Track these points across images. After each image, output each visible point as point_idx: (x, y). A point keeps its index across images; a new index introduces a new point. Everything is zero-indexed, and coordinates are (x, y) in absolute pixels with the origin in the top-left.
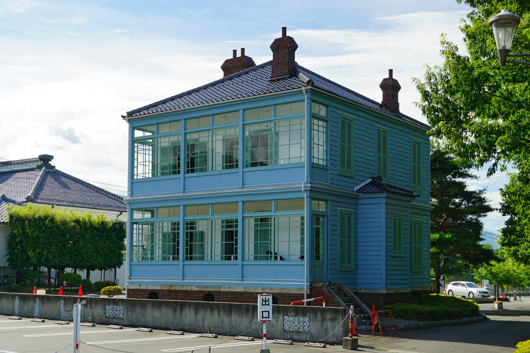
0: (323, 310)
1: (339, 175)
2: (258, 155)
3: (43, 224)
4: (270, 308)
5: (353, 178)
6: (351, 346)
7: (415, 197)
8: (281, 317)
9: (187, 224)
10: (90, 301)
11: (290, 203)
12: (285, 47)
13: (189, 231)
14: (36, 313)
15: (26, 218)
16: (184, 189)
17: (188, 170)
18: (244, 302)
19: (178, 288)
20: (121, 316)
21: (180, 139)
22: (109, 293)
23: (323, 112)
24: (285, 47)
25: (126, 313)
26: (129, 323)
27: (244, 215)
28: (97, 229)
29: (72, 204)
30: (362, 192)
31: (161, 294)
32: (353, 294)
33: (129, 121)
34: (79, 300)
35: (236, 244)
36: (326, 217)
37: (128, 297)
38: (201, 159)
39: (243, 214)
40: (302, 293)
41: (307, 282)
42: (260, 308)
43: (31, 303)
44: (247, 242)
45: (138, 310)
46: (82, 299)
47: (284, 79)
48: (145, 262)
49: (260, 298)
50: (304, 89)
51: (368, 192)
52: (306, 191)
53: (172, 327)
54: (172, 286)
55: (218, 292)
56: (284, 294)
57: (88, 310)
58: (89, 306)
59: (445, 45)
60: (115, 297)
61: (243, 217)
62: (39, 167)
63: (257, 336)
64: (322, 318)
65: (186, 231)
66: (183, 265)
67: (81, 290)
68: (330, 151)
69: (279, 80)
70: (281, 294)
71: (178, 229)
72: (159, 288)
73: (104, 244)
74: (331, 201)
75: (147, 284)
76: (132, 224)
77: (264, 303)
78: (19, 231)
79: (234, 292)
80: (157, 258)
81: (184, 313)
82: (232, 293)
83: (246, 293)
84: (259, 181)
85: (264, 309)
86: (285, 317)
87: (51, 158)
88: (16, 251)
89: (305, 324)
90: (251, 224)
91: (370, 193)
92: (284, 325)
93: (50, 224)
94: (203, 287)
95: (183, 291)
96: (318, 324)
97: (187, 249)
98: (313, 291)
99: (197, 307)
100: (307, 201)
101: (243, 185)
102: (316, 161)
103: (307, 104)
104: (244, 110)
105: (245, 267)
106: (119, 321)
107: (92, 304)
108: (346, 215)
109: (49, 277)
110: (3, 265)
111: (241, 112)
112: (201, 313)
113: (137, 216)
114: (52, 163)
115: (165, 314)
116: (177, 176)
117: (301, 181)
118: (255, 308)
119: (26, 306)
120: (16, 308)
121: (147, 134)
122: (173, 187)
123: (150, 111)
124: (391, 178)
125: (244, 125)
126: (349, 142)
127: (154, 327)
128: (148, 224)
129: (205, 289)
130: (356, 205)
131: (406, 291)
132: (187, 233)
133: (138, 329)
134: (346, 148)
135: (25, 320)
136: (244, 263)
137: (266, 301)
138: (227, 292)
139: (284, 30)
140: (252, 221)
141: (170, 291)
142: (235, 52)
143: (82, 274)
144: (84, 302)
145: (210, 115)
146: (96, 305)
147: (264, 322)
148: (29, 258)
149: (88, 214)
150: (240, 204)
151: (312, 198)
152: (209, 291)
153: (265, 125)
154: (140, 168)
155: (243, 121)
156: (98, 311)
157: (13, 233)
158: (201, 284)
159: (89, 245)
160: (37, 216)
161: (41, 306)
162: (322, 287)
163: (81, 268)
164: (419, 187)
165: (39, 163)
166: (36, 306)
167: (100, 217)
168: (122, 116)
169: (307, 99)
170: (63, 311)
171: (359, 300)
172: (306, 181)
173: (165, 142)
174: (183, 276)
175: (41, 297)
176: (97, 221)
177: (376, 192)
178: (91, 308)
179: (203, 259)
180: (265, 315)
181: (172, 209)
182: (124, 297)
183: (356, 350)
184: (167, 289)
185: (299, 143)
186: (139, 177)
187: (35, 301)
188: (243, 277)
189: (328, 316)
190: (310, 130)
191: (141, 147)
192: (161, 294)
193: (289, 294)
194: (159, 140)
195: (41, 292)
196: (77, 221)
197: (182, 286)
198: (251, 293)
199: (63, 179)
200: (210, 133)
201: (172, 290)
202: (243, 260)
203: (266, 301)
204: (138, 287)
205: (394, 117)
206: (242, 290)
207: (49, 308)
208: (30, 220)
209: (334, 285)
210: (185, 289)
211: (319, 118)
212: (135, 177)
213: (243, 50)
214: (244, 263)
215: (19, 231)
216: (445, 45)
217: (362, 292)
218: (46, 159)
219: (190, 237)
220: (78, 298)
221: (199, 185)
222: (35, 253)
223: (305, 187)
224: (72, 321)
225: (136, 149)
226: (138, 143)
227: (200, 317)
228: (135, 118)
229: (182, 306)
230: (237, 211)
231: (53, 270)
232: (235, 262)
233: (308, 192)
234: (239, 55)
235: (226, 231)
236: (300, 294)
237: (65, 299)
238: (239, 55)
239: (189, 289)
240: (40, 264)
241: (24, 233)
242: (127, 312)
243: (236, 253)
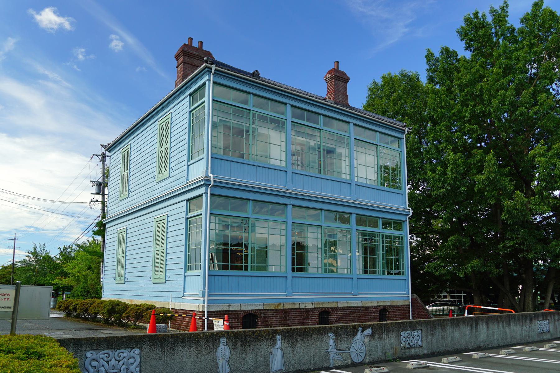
20: (420, 343)
25: (424, 338)
31: (262, 315)
34: (360, 329)
40: (407, 304)
46: (364, 328)
54: (280, 304)
55: (334, 308)
58: (377, 336)
60: (497, 309)
89: (132, 360)
95: (294, 309)
107: (382, 332)
129: (321, 306)
138: (345, 307)
144: (369, 331)
152: (384, 306)
161: (289, 350)
166: (275, 351)
170: (332, 349)
178: (380, 339)
179: (293, 270)
184: (273, 308)
187: (274, 342)
192: (262, 315)
198: (367, 307)
201: (279, 310)
210: (297, 307)
220: (359, 326)
236: (406, 305)
237: (284, 334)
239: (302, 306)
242: (427, 336)
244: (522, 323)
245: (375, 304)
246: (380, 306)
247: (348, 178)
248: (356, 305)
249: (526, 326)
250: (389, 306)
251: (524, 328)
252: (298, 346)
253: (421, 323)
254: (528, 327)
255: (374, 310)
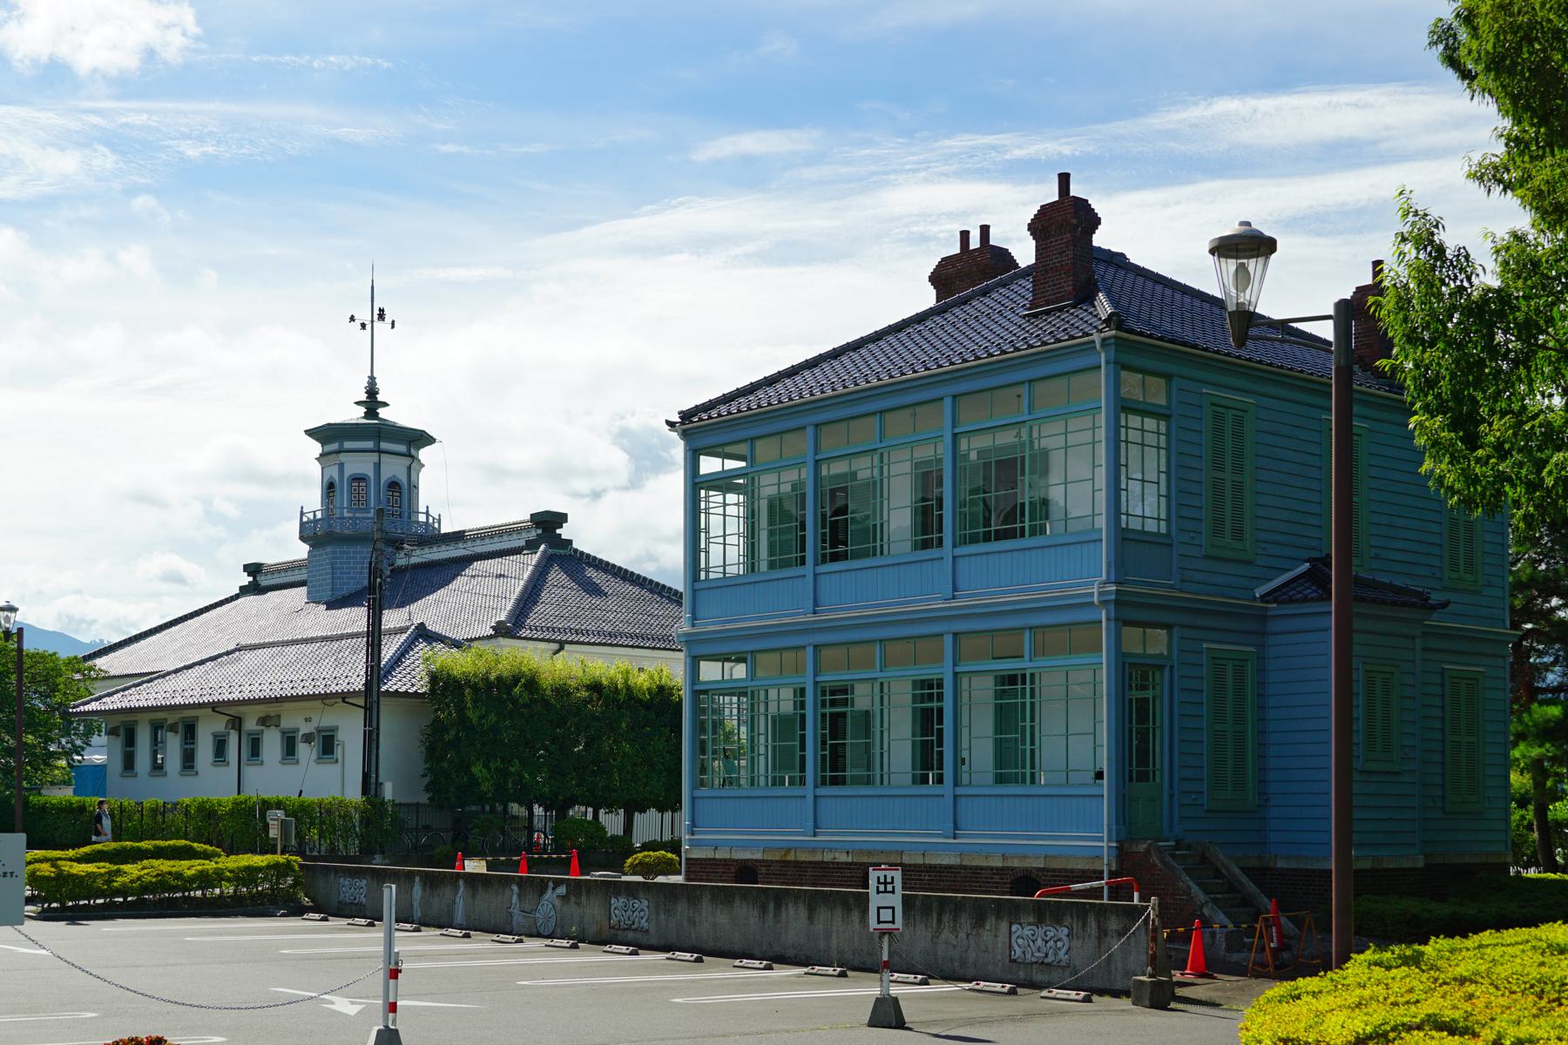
0: (1102, 911)
1: (1207, 557)
2: (1001, 509)
3: (511, 697)
4: (896, 900)
5: (1250, 563)
6: (1151, 1000)
7: (1433, 608)
8: (1004, 925)
9: (824, 693)
10: (576, 888)
11: (1060, 631)
12: (1065, 222)
13: (828, 710)
14: (459, 917)
15: (468, 682)
16: (816, 604)
17: (824, 556)
18: (840, 883)
19: (803, 857)
21: (803, 476)
22: (645, 869)
23: (1157, 394)
24: (1065, 222)
26: (662, 942)
27: (958, 669)
28: (647, 706)
29: (611, 640)
30: (1275, 601)
32: (1237, 871)
33: (685, 435)
34: (551, 885)
35: (940, 744)
36: (1167, 670)
37: (687, 879)
38: (784, 537)
39: (955, 665)
41: (1109, 840)
42: (875, 900)
43: (448, 891)
44: (977, 739)
45: (682, 907)
46: (557, 883)
47: (1060, 309)
48: (778, 791)
49: (873, 875)
50: (1096, 337)
51: (1291, 601)
52: (1104, 603)
53: (756, 952)
54: (789, 850)
56: (1054, 870)
57: (572, 909)
58: (573, 899)
59: (1411, 218)
60: (660, 879)
61: (956, 674)
62: (531, 546)
63: (869, 966)
64: (1099, 928)
65: (820, 711)
66: (816, 797)
67: (575, 862)
68: (1178, 495)
69: (1047, 313)
70: (1048, 870)
71: (940, 697)
72: (759, 856)
73: (633, 742)
74: (1181, 626)
75: (732, 845)
76: (696, 694)
77: (882, 888)
78: (450, 714)
79: (935, 866)
80: (762, 779)
81: (784, 915)
82: (931, 868)
83: (965, 867)
84: (1000, 578)
85: (885, 901)
86: (1014, 928)
87: (561, 518)
88: (445, 765)
89: (1059, 944)
90: (982, 691)
91: (1297, 601)
92: (1010, 946)
93: (526, 695)
94: (861, 852)
96: (1091, 943)
97: (824, 757)
98: (1131, 867)
99: (813, 902)
100: (1108, 629)
101: (955, 589)
102: (1135, 524)
103: (1107, 376)
104: (954, 397)
105: (962, 802)
106: (639, 935)
108: (1230, 665)
109: (530, 829)
110: (414, 801)
111: (948, 402)
112: (822, 914)
113: (710, 671)
114: (565, 532)
115: (744, 919)
116: (798, 571)
117: (1092, 577)
118: (863, 901)
119: (436, 901)
120: (416, 904)
121: (731, 464)
122: (786, 602)
123: (714, 413)
124: (1377, 557)
125: (955, 435)
126: (1238, 468)
127: (705, 951)
128: (740, 695)
130: (1264, 633)
131: (1406, 864)
132: (824, 715)
133: (669, 955)
134: (1228, 485)
135: (428, 932)
136: (959, 791)
137: (885, 883)
139: (1064, 179)
140: (989, 683)
141: (785, 864)
142: (965, 235)
143: (612, 823)
144: (562, 890)
145: (874, 413)
146: (588, 899)
147: (883, 933)
148: (474, 782)
149: (623, 665)
150: (948, 639)
151: (1121, 622)
152: (1026, 869)
153: (1014, 432)
154: (716, 551)
155: (954, 426)
156: (592, 911)
157: (436, 720)
158: (857, 847)
159: (627, 747)
160: (492, 677)
162: (1148, 850)
163: (611, 807)
164: (1469, 577)
165: (533, 535)
167: (656, 678)
168: (669, 423)
169: (1107, 362)
170: (516, 911)
171: (1252, 887)
172: (1104, 577)
173: (769, 486)
174: (816, 826)
175: (473, 879)
176: (646, 685)
177: (1312, 600)
178: (578, 904)
180: (886, 915)
181: (787, 656)
182: (678, 879)
183: (1164, 1008)
185: (1094, 473)
186: (712, 576)
187: (457, 888)
188: (956, 827)
189: (1113, 924)
190: (1116, 443)
191: (716, 497)
193: (1066, 870)
194: (1035, 429)
195: (475, 866)
196: (595, 687)
197: (814, 851)
198: (977, 868)
199: (591, 572)
200: (876, 458)
202: (956, 784)
203: (885, 883)
204: (711, 855)
205: (1372, 391)
206: (952, 860)
207: (487, 903)
208: (475, 687)
209: (1189, 847)
210: (818, 858)
211: (1145, 412)
212: (703, 575)
213: (985, 230)
214: (959, 791)
215: (450, 714)
216: (1411, 218)
217: (1279, 865)
218: (548, 523)
219: (836, 725)
221: (854, 593)
222: (489, 770)
223: (1100, 594)
224: (380, 919)
225: (703, 505)
226: (708, 489)
227: (819, 927)
228: (700, 427)
229: (780, 898)
230: (939, 658)
231: (538, 810)
232: (938, 790)
233: (1112, 607)
234: (975, 243)
235: (831, 714)
238: (975, 243)
239: (828, 857)
240: (503, 796)
241: (463, 719)
243: (941, 767)
244: (939, 921)
245: (997, 863)
246: (1013, 869)
247: (1163, 530)
248: (946, 862)
249: (954, 930)
250: (1043, 869)
251: (946, 934)
252: (478, 897)
253: (744, 894)
254: (962, 935)
255: (997, 878)
